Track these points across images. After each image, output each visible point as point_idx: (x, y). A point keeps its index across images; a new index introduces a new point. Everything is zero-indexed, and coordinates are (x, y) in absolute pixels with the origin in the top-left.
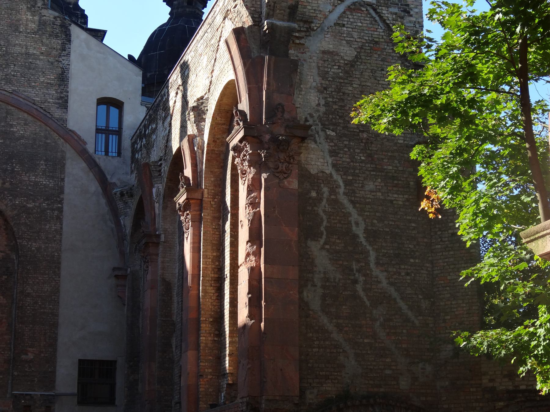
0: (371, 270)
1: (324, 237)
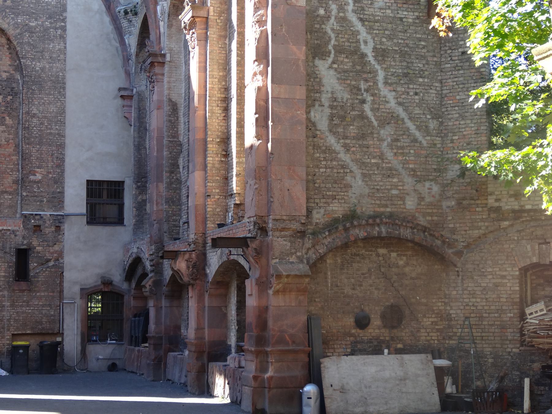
0: (379, 90)
1: (332, 55)
